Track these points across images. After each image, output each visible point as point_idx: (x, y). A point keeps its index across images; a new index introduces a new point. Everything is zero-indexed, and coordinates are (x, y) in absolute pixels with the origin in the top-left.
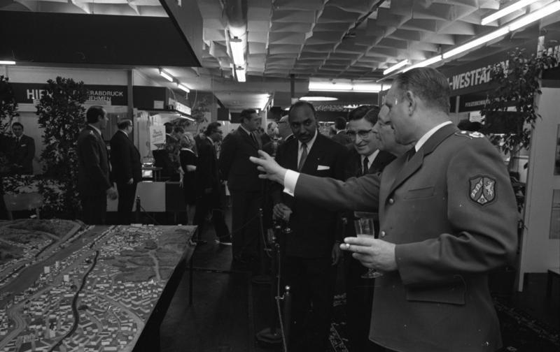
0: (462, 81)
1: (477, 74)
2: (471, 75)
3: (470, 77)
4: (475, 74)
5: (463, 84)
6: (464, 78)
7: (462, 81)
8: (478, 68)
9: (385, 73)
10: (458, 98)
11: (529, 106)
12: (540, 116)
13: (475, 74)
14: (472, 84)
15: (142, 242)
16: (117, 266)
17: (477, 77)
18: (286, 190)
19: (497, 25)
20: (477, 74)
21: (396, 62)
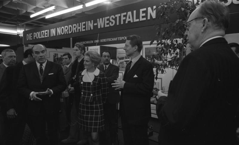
0: (107, 22)
1: (45, 32)
2: (116, 18)
3: (115, 19)
4: (120, 17)
5: (107, 24)
6: (108, 20)
7: (107, 22)
8: (46, 30)
9: (32, 16)
10: (71, 38)
11: (172, 47)
12: (165, 71)
13: (120, 17)
14: (118, 24)
15: (171, 64)
16: (158, 133)
17: (123, 18)
18: (7, 112)
19: (54, 11)
20: (45, 32)
21: (34, 12)
